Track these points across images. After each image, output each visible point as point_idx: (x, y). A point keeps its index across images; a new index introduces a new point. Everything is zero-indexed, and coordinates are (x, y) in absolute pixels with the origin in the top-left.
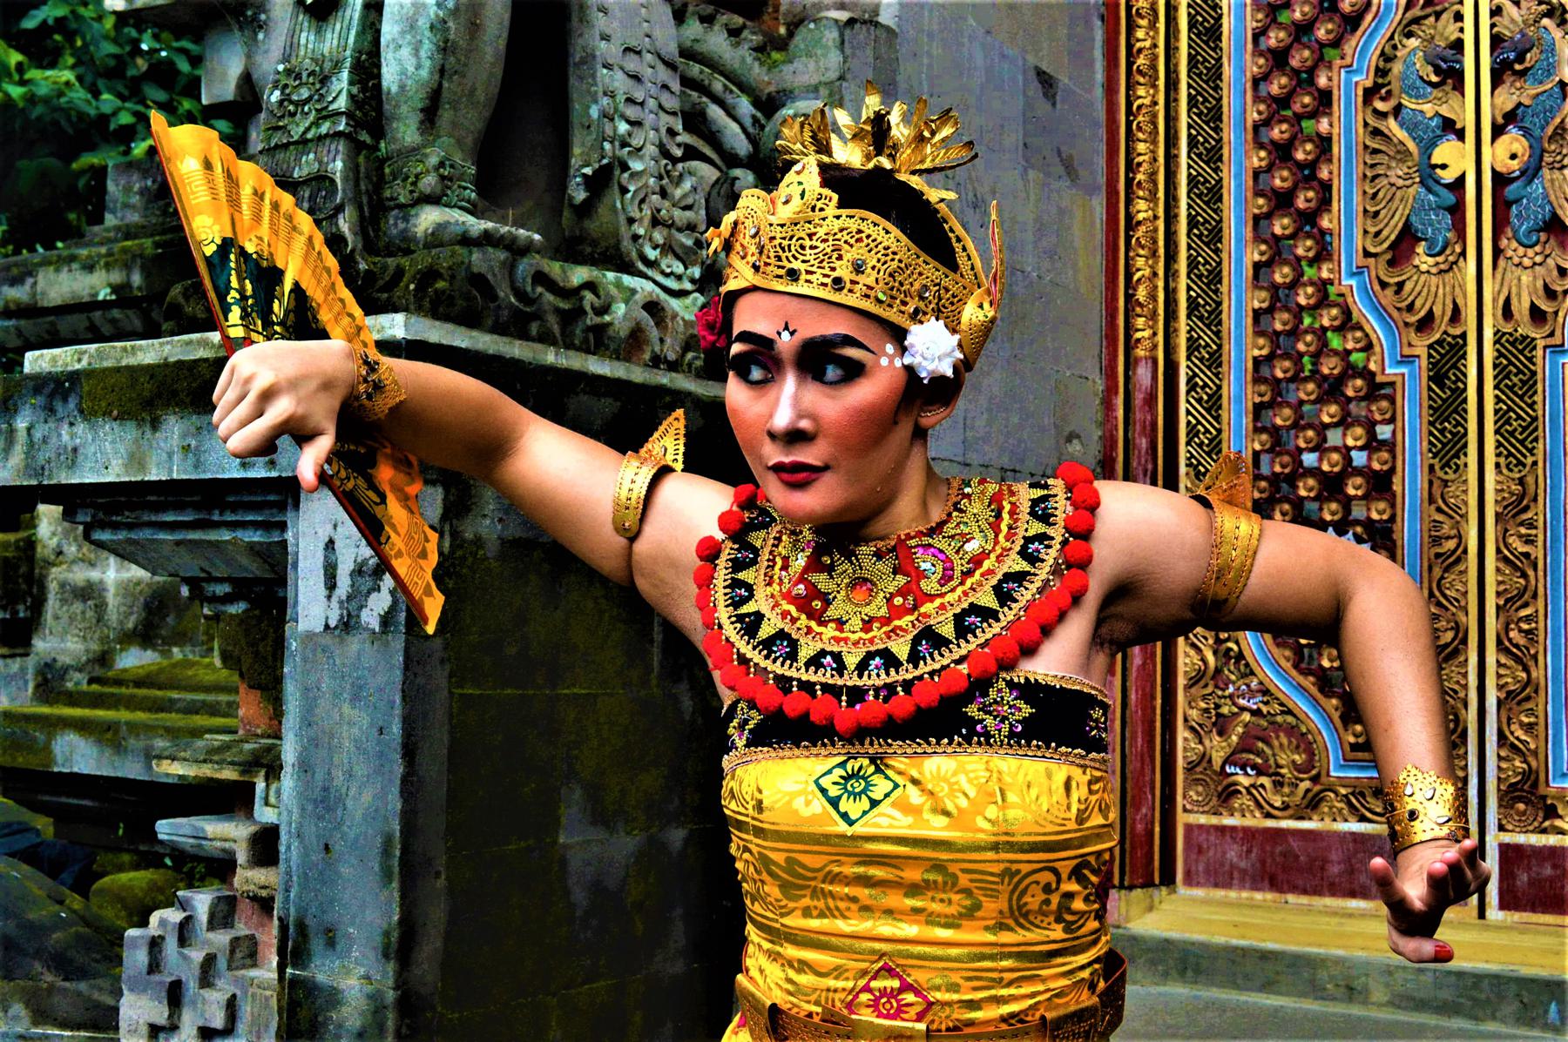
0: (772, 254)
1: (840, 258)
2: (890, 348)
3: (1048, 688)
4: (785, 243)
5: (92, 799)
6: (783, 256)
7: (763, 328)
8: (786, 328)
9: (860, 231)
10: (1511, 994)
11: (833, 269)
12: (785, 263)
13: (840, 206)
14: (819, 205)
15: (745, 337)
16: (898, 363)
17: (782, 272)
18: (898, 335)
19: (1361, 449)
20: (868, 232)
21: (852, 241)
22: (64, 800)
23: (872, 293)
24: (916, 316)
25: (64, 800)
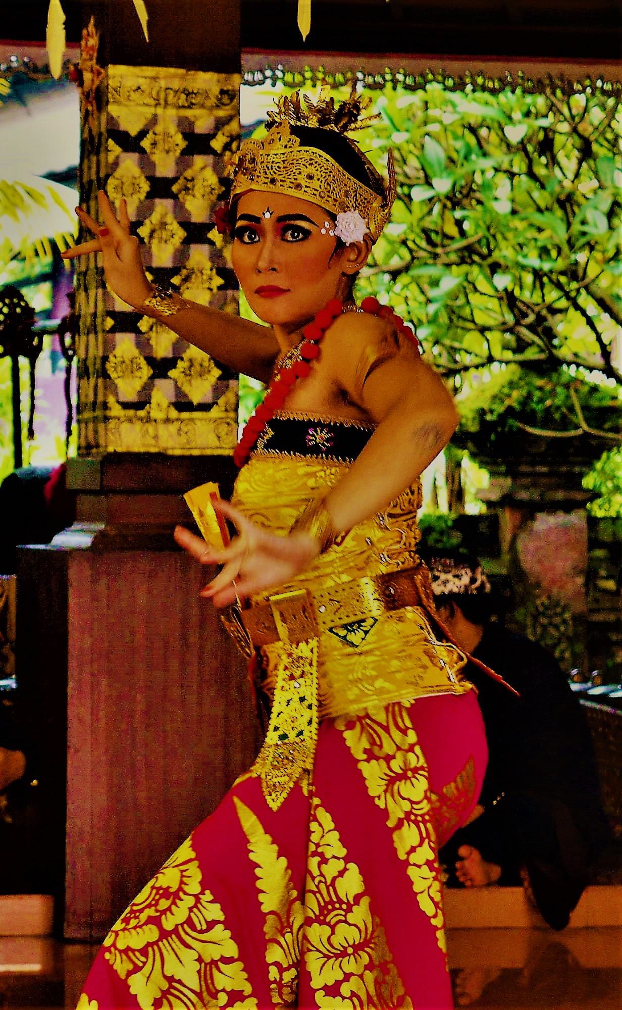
0: (262, 171)
1: (300, 173)
2: (327, 225)
3: (486, 781)
4: (269, 165)
5: (29, 550)
6: (268, 172)
7: (254, 211)
8: (268, 211)
9: (311, 159)
10: (494, 407)
11: (296, 179)
12: (269, 176)
13: (301, 144)
14: (289, 144)
15: (245, 217)
16: (332, 234)
17: (266, 180)
18: (333, 217)
19: (457, 788)
20: (316, 160)
21: (307, 164)
22: (32, 547)
23: (317, 193)
24: (344, 209)
25: (32, 547)
